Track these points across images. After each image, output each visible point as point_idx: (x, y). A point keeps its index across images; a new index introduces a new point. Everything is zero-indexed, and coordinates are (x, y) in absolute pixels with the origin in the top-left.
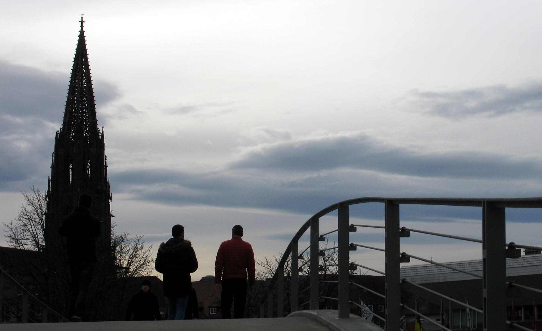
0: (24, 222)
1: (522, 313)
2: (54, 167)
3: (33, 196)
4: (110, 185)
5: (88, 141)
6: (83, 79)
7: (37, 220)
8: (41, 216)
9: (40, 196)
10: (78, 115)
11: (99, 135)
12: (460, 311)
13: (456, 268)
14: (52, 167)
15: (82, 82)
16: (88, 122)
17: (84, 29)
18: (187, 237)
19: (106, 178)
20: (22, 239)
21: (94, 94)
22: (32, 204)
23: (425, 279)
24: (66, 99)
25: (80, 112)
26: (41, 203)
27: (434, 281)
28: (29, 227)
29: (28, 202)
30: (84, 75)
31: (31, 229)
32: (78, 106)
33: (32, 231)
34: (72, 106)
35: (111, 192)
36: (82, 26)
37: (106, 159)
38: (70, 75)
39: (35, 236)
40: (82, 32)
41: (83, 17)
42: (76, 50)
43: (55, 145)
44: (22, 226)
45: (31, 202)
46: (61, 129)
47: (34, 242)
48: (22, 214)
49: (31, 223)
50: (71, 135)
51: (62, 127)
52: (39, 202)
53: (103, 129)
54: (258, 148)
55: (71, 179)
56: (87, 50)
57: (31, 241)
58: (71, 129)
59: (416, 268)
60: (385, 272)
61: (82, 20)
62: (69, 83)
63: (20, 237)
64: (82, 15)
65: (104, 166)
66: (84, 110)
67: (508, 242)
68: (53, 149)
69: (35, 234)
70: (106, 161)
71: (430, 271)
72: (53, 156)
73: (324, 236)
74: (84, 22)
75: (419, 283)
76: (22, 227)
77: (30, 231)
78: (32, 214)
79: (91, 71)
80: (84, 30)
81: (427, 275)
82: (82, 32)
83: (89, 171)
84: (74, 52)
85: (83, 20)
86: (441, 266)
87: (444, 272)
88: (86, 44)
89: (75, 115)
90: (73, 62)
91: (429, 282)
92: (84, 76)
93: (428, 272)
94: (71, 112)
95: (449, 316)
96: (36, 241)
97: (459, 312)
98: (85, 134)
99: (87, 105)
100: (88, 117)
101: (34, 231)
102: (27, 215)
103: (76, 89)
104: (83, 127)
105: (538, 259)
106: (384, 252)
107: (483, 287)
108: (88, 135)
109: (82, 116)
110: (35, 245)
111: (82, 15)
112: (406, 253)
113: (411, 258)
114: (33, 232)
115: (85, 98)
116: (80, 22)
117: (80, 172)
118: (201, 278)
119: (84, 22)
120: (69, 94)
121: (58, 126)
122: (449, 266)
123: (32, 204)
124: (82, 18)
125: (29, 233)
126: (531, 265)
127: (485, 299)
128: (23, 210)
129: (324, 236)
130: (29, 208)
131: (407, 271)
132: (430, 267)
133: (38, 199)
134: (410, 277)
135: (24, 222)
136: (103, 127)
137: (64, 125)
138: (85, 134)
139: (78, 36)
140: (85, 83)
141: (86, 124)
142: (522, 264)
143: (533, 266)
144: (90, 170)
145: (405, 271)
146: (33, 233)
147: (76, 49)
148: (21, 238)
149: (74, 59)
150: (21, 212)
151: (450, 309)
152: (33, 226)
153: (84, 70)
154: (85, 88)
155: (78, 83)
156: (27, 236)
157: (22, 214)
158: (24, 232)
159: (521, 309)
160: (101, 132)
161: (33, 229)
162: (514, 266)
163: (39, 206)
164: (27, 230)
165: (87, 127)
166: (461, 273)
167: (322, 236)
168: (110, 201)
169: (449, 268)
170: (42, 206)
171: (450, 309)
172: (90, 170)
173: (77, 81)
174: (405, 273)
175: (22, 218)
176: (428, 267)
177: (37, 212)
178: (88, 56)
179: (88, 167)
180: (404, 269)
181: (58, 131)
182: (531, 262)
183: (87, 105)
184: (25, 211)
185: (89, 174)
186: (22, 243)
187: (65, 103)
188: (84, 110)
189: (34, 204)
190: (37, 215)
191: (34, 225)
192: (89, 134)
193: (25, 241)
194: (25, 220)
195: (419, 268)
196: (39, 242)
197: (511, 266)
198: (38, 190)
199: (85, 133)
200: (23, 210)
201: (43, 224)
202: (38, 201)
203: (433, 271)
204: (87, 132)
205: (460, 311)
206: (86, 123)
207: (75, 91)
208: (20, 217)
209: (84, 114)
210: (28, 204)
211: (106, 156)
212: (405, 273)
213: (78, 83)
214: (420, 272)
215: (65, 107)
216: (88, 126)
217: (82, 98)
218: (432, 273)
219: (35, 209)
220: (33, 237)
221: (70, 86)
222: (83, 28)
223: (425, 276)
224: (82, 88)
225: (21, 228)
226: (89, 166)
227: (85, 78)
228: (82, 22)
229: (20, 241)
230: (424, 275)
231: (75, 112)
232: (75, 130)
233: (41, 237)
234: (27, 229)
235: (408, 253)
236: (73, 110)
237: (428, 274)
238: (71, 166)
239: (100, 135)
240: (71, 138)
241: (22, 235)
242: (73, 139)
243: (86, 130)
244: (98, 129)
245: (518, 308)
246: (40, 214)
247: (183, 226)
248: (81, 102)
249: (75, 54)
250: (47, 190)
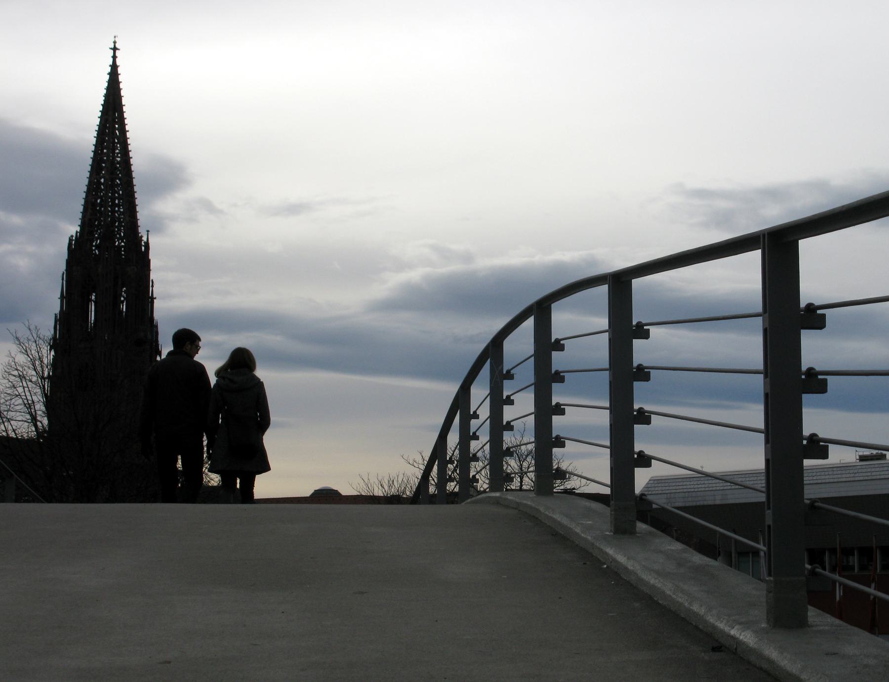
0: (11, 382)
1: (854, 560)
2: (65, 298)
3: (28, 338)
4: (159, 330)
5: (123, 255)
6: (115, 148)
7: (34, 379)
8: (41, 372)
9: (39, 338)
10: (106, 208)
11: (141, 245)
12: (751, 555)
13: (739, 480)
15: (114, 153)
16: (122, 222)
17: (118, 62)
19: (152, 318)
20: (8, 411)
21: (134, 175)
22: (26, 351)
23: (690, 499)
24: (86, 182)
25: (110, 204)
26: (42, 349)
27: (706, 503)
28: (20, 390)
29: (19, 348)
30: (116, 141)
31: (23, 394)
32: (106, 195)
33: (25, 398)
34: (96, 194)
35: (160, 343)
36: (114, 57)
37: (152, 286)
38: (94, 141)
39: (29, 406)
40: (114, 67)
41: (116, 40)
42: (104, 98)
43: (67, 260)
44: (9, 388)
45: (24, 348)
46: (77, 232)
47: (28, 417)
48: (8, 367)
49: (24, 383)
50: (94, 244)
51: (78, 229)
52: (38, 349)
53: (148, 234)
54: (415, 275)
55: (93, 318)
56: (123, 98)
57: (23, 414)
58: (95, 233)
59: (674, 480)
60: (610, 484)
61: (115, 46)
62: (92, 155)
63: (5, 406)
64: (115, 37)
65: (149, 297)
66: (117, 202)
67: (806, 432)
68: (63, 267)
69: (30, 402)
70: (152, 289)
71: (700, 486)
72: (63, 279)
73: (512, 424)
74: (119, 49)
75: (680, 505)
76: (8, 389)
77: (22, 397)
78: (26, 368)
79: (128, 135)
80: (118, 63)
81: (694, 492)
82: (114, 67)
83: (125, 306)
84: (101, 100)
85: (117, 46)
86: (714, 477)
87: (722, 488)
88: (121, 88)
89: (100, 208)
90: (99, 117)
91: (698, 504)
92: (117, 143)
93: (696, 486)
94: (94, 204)
95: (732, 561)
96: (31, 415)
97: (749, 557)
98: (117, 243)
99: (121, 192)
100: (123, 213)
101: (29, 398)
102: (17, 370)
103: (104, 165)
104: (115, 231)
105: (881, 469)
106: (609, 450)
108: (123, 244)
109: (113, 212)
110: (30, 421)
111: (115, 37)
112: (644, 452)
113: (652, 460)
114: (27, 399)
115: (117, 181)
116: (111, 49)
117: (108, 307)
118: (312, 492)
119: (119, 49)
120: (91, 172)
121: (73, 229)
122: (728, 478)
123: (26, 351)
124: (115, 42)
125: (20, 401)
126: (869, 478)
127: (769, 527)
128: (11, 361)
129: (512, 424)
130: (21, 359)
131: (660, 485)
132: (698, 479)
133: (36, 342)
134: (666, 495)
135: (11, 382)
136: (148, 231)
137: (82, 226)
138: (117, 243)
139: (108, 74)
140: (119, 155)
141: (120, 226)
142: (854, 477)
143: (880, 479)
144: (125, 304)
145: (656, 485)
146: (28, 400)
147: (104, 96)
148: (6, 409)
149: (100, 113)
150: (7, 364)
151: (733, 551)
152: (26, 389)
153: (117, 131)
154: (118, 163)
155: (107, 155)
156: (17, 405)
157: (8, 367)
158: (11, 399)
159: (854, 555)
160: (145, 239)
161: (28, 394)
162: (840, 480)
163: (37, 356)
164: (17, 396)
165: (120, 230)
166: (747, 490)
167: (508, 423)
169: (727, 481)
170: (43, 356)
171: (733, 551)
172: (125, 304)
173: (105, 151)
174: (656, 489)
175: (9, 375)
176: (695, 479)
177: (34, 365)
178: (125, 109)
179: (122, 299)
180: (656, 482)
181: (72, 236)
182: (869, 474)
183: (121, 192)
184: (13, 363)
185: (124, 310)
186: (8, 417)
187: (85, 189)
188: (117, 202)
189: (29, 351)
190: (35, 370)
191: (28, 387)
192: (124, 243)
193: (14, 413)
194: (14, 378)
195: (680, 480)
196: (36, 417)
197: (836, 480)
198: (36, 328)
199: (118, 241)
200: (11, 361)
201: (44, 386)
202: (37, 346)
203: (703, 486)
204: (121, 239)
205: (751, 555)
206: (120, 223)
207: (102, 169)
208: (6, 373)
209: (117, 209)
210: (20, 350)
211: (152, 280)
212: (656, 489)
213: (107, 155)
214: (681, 487)
215: (84, 195)
216: (122, 228)
217: (113, 180)
218: (703, 489)
219: (31, 359)
220: (27, 408)
221: (95, 152)
222: (117, 60)
223: (687, 493)
224: (113, 163)
225: (8, 392)
226: (124, 297)
227: (118, 146)
228: (115, 49)
229: (5, 413)
230: (688, 492)
231: (101, 205)
232: (101, 234)
233: (40, 407)
234: (17, 394)
235: (648, 452)
236: (99, 201)
237: (696, 490)
238: (93, 297)
239: (143, 244)
240: (94, 248)
241: (8, 403)
242: (97, 251)
243: (120, 234)
244: (140, 235)
245: (847, 552)
246: (39, 368)
248: (111, 187)
249: (102, 105)
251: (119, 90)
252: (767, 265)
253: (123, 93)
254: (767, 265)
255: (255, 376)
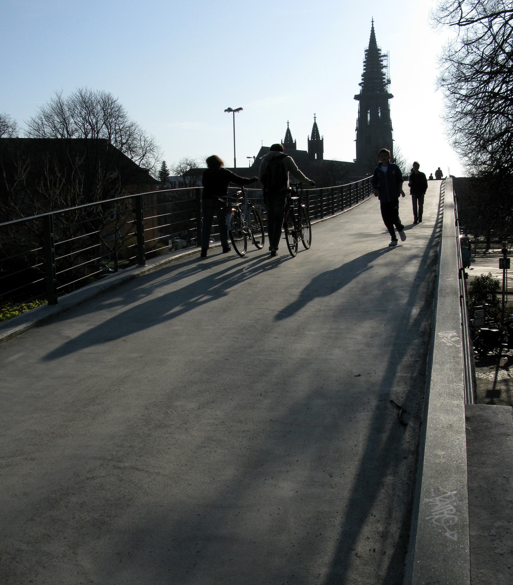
14: (359, 112)
17: (374, 26)
18: (441, 169)
36: (373, 25)
40: (373, 28)
80: (374, 27)
82: (373, 28)
85: (373, 20)
107: (54, 253)
117: (374, 115)
124: (373, 19)
168: (392, 131)
222: (374, 25)
228: (373, 22)
247: (443, 173)
250: (356, 126)
251: (374, 34)
252: (466, 317)
253: (376, 37)
254: (466, 317)
255: (358, 100)
